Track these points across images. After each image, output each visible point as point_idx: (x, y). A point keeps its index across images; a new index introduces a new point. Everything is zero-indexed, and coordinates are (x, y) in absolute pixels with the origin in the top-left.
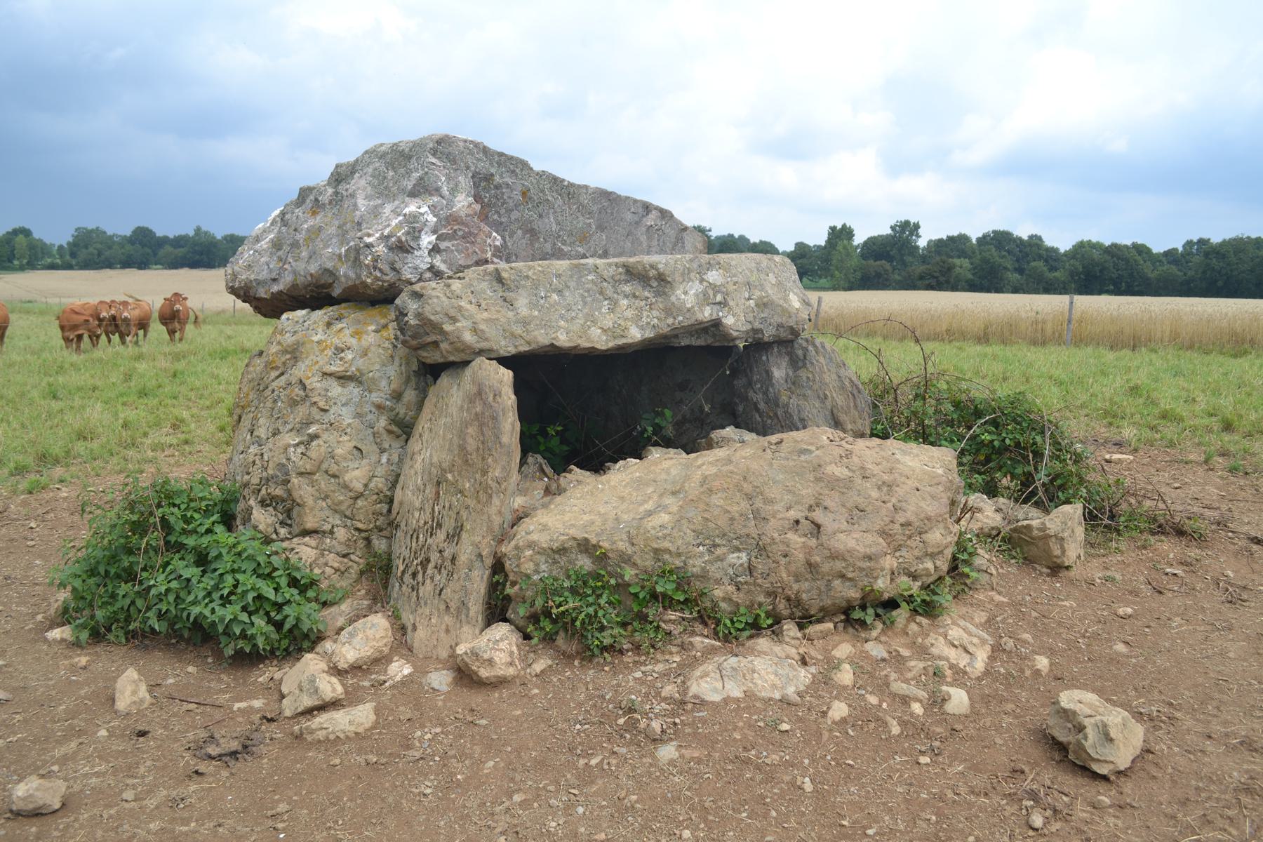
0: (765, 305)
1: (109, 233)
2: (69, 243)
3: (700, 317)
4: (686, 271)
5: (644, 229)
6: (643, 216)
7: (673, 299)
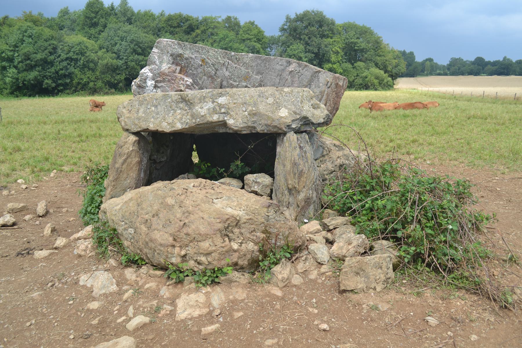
0: (255, 114)
1: (465, 60)
2: (448, 65)
3: (210, 119)
5: (288, 73)
6: (287, 66)
7: (194, 111)
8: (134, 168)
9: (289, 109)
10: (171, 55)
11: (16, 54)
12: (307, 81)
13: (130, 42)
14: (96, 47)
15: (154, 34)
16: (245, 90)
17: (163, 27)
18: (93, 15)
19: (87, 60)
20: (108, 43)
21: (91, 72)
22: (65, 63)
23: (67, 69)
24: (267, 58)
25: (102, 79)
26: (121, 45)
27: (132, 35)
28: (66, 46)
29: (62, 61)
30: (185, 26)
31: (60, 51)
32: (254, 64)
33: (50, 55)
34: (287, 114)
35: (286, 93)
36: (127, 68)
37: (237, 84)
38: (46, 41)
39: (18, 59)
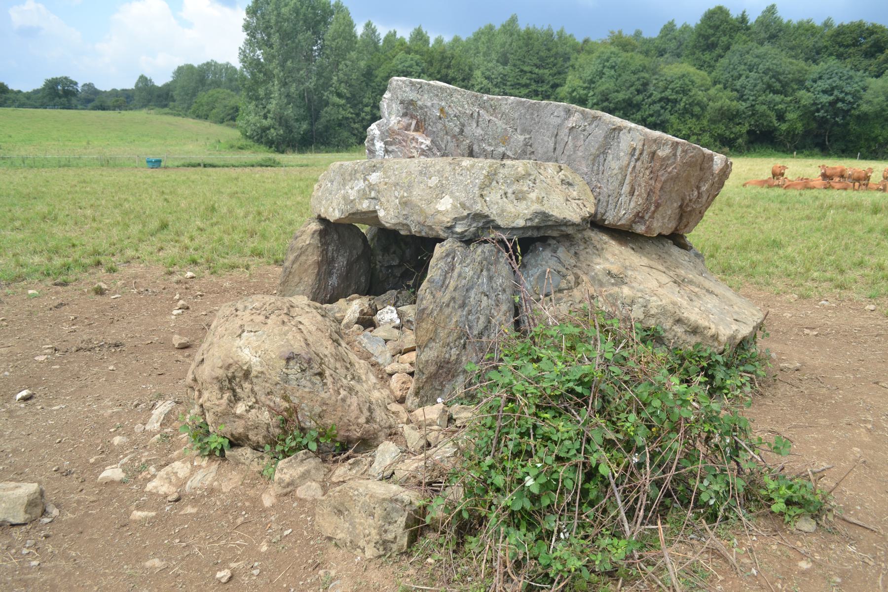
3: (360, 208)
4: (353, 172)
5: (567, 131)
8: (310, 271)
9: (456, 198)
10: (402, 102)
11: (591, 93)
12: (597, 146)
13: (763, 73)
14: (709, 81)
15: (806, 60)
16: (406, 162)
17: (826, 47)
18: (711, 31)
19: (690, 101)
20: (728, 75)
21: (694, 120)
22: (657, 107)
23: (660, 115)
24: (535, 104)
25: (710, 131)
26: (747, 77)
27: (768, 61)
28: (662, 81)
29: (654, 102)
30: (866, 44)
31: (652, 88)
32: (516, 115)
33: (638, 94)
34: (449, 206)
35: (462, 170)
36: (753, 114)
37: (492, 149)
38: (634, 73)
39: (593, 99)
